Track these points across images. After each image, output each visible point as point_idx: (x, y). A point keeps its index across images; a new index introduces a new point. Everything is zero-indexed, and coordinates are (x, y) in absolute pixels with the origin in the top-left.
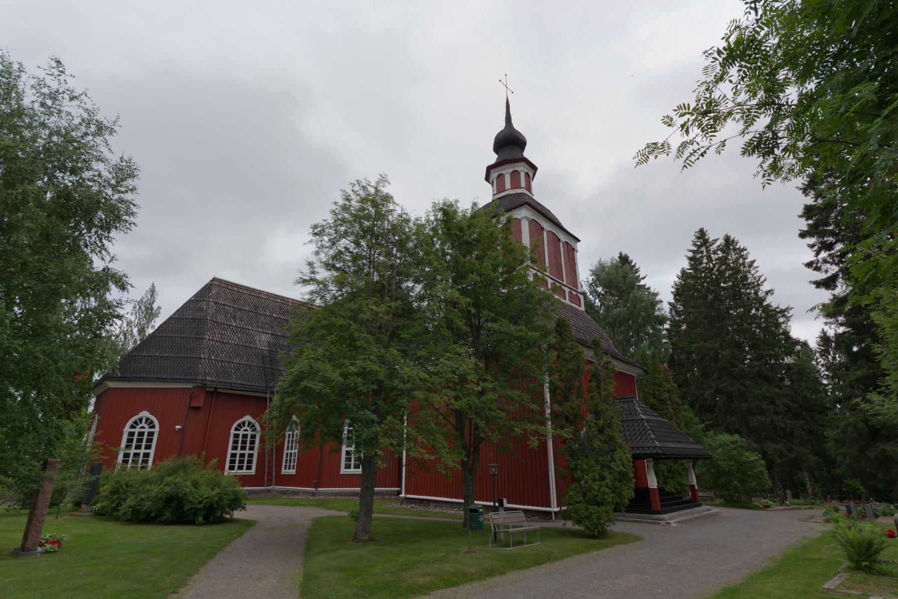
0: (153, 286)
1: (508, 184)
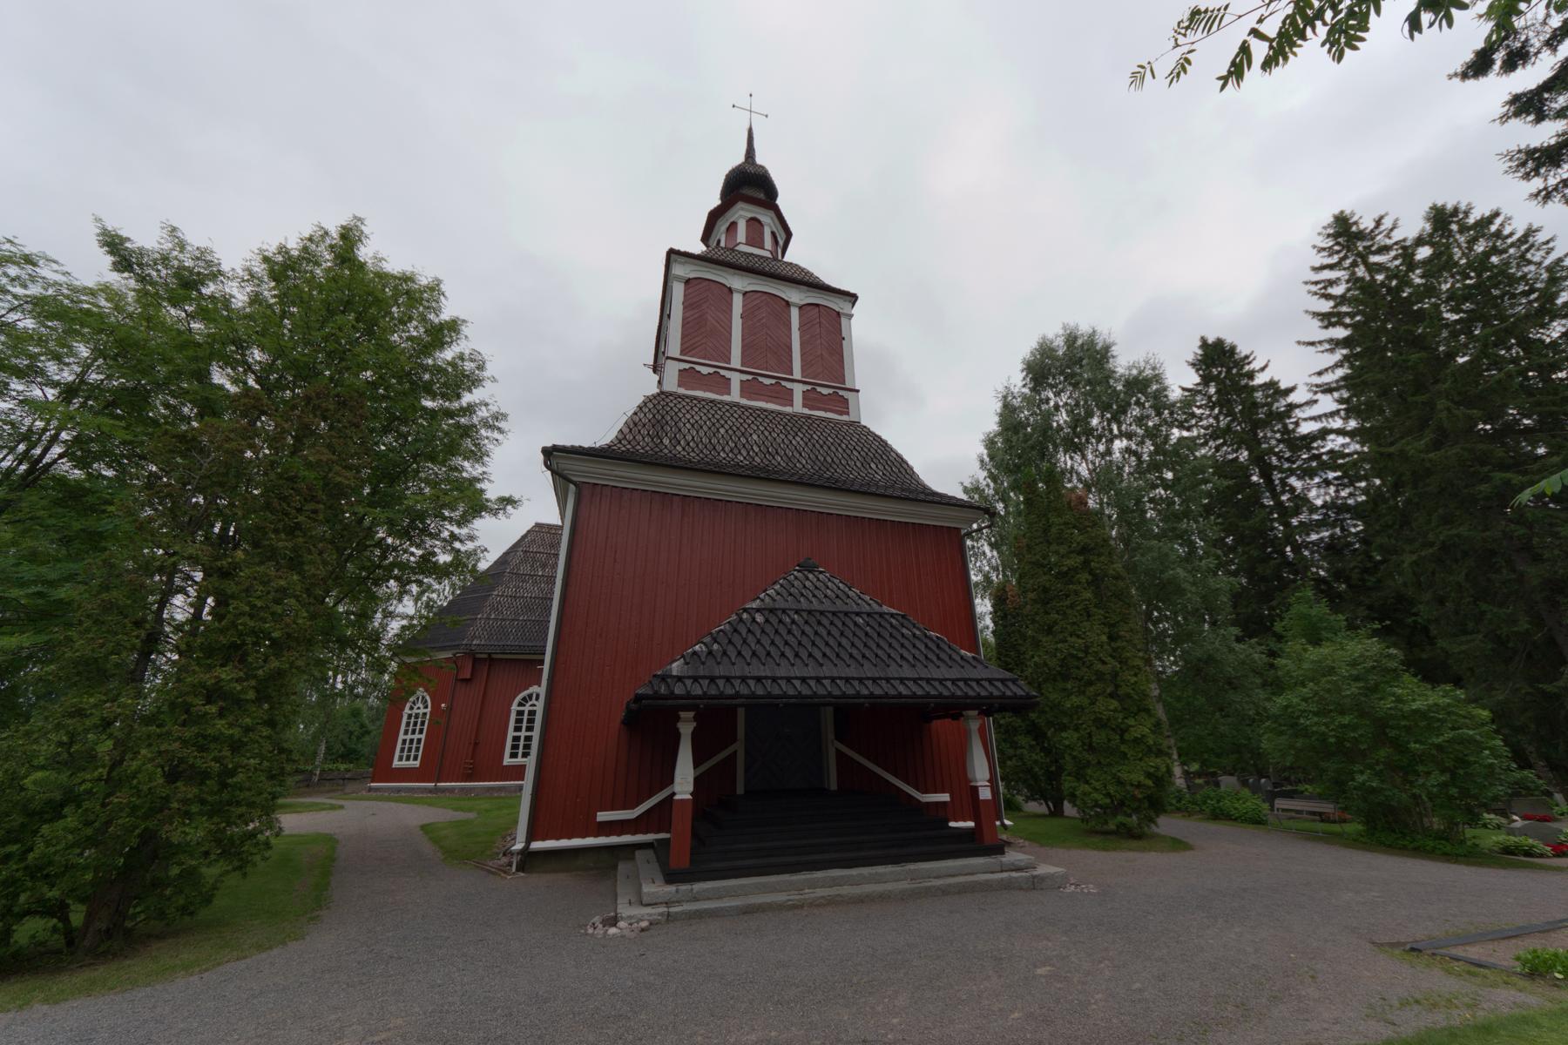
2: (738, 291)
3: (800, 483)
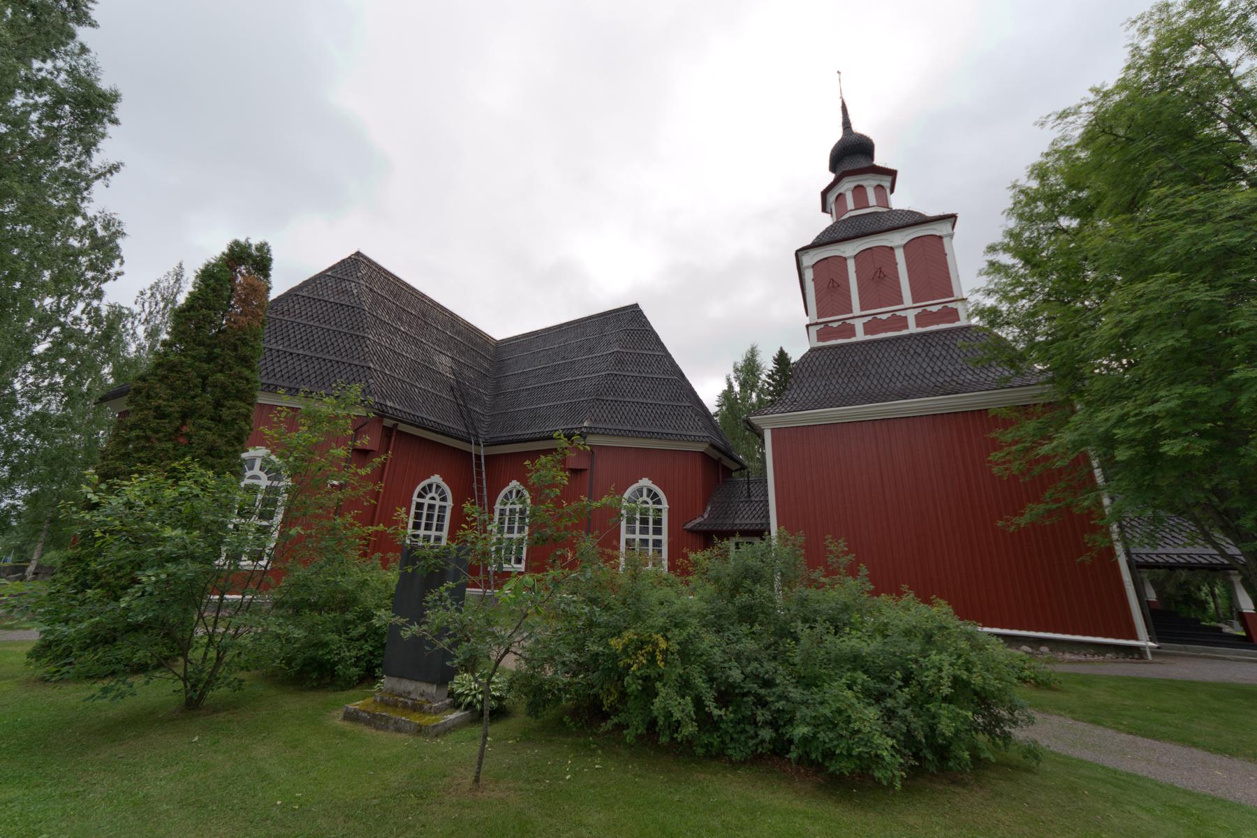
0: (180, 266)
1: (850, 204)
2: (899, 247)
3: (452, 437)
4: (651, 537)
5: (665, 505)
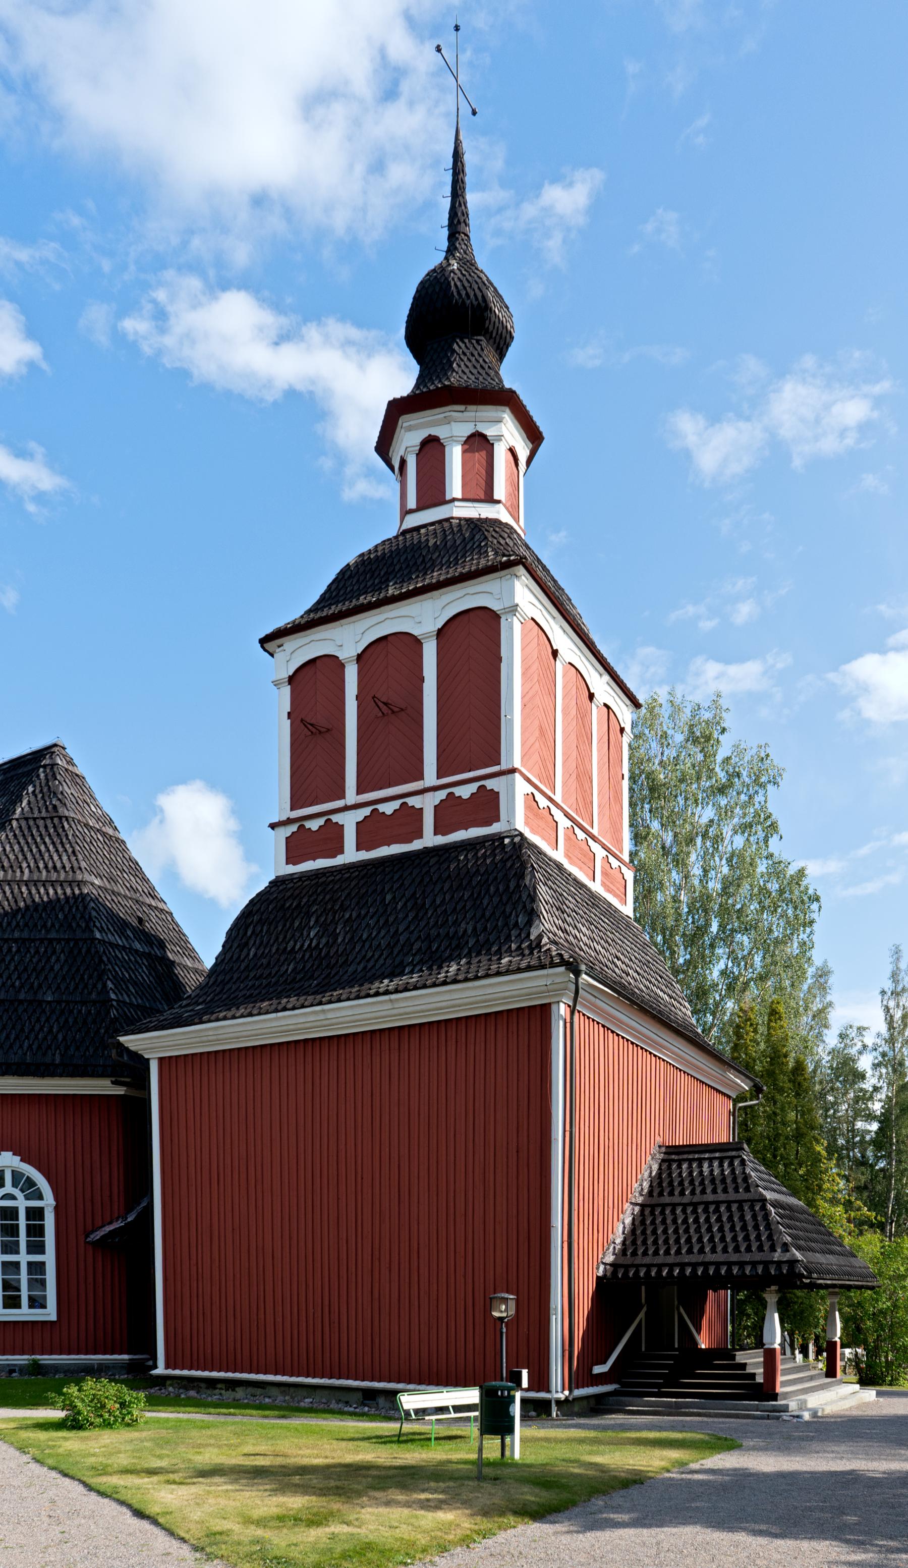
2: (428, 636)
4: (23, 1258)
5: (48, 1201)
